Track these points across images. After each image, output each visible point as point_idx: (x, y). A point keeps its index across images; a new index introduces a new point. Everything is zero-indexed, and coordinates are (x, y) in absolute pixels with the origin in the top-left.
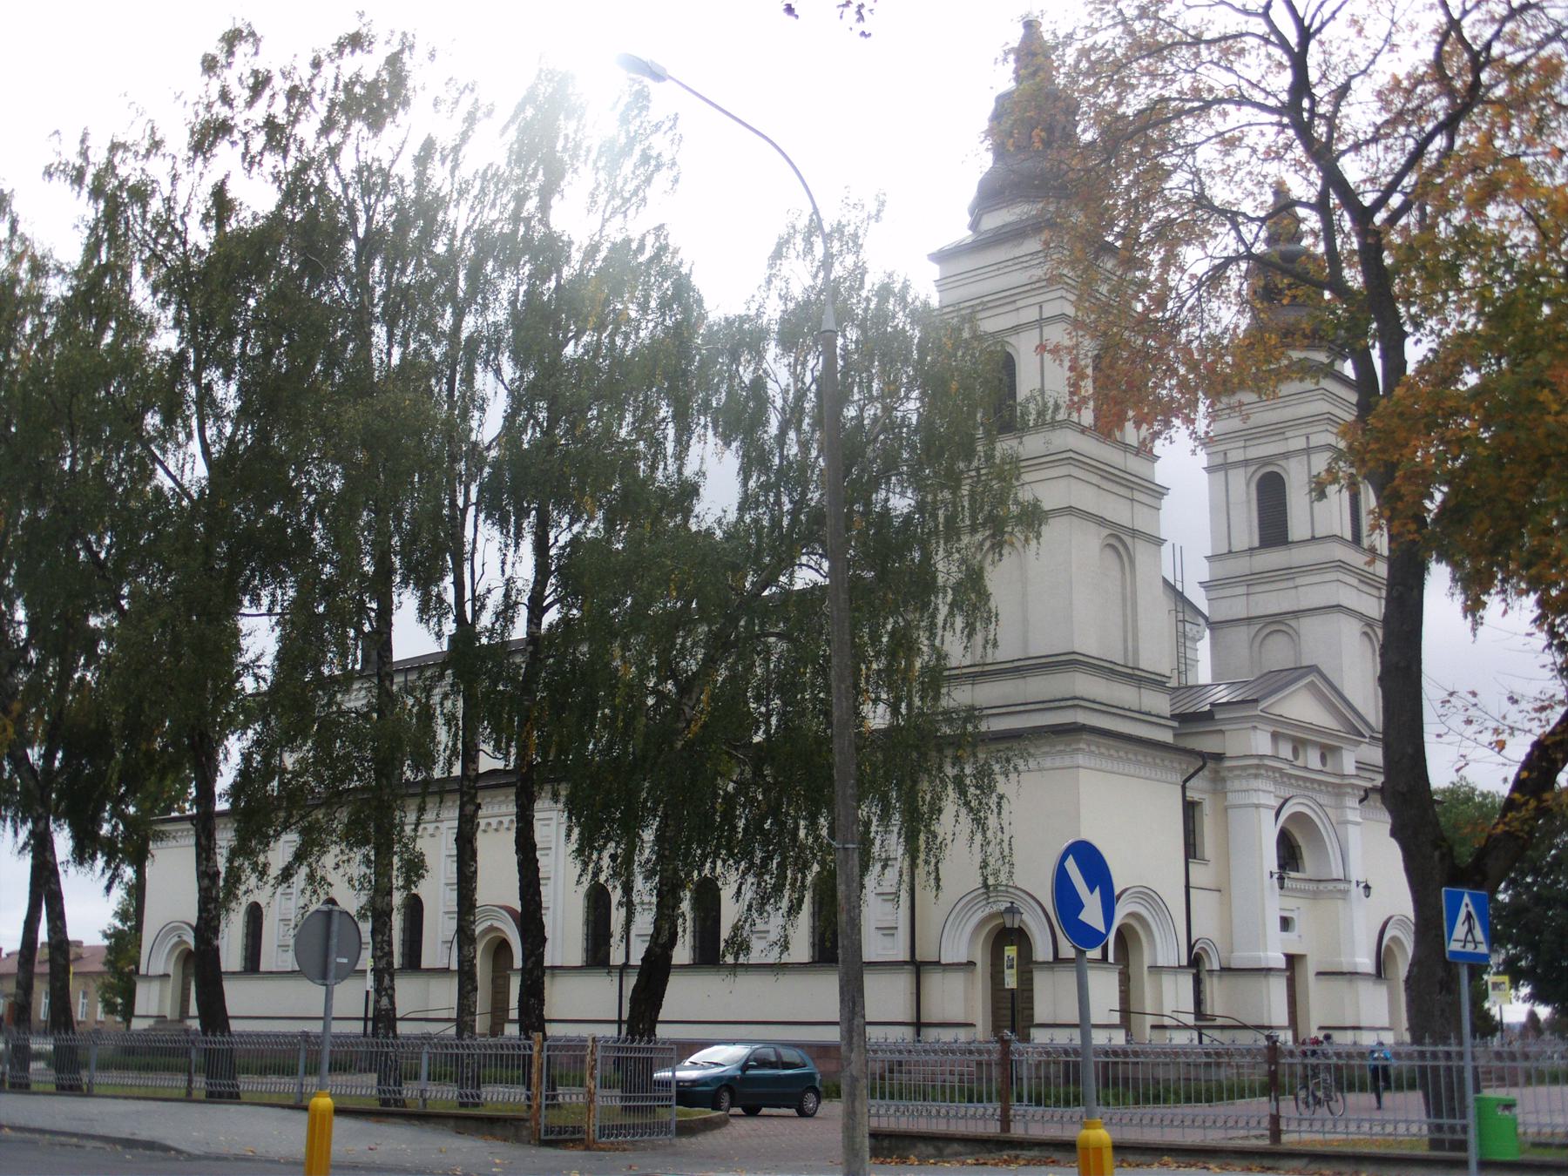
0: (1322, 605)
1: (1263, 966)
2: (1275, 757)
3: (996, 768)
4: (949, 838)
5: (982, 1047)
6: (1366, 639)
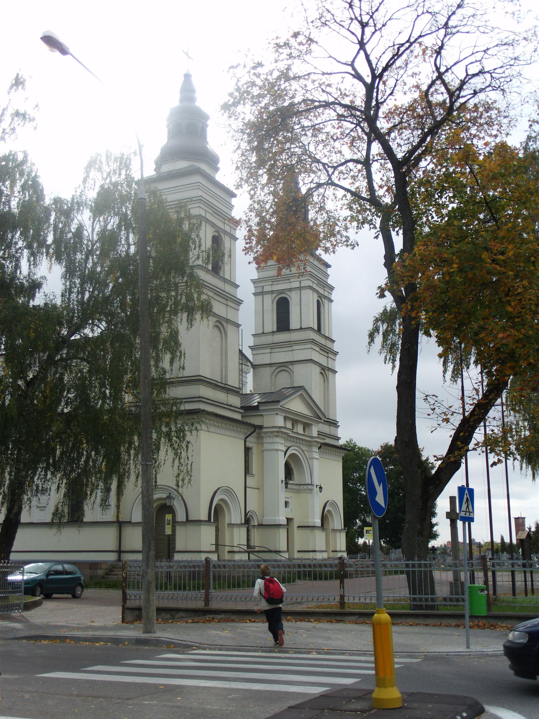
0: (304, 359)
1: (277, 523)
2: (285, 428)
3: (186, 428)
4: (163, 462)
5: (195, 564)
6: (321, 375)
